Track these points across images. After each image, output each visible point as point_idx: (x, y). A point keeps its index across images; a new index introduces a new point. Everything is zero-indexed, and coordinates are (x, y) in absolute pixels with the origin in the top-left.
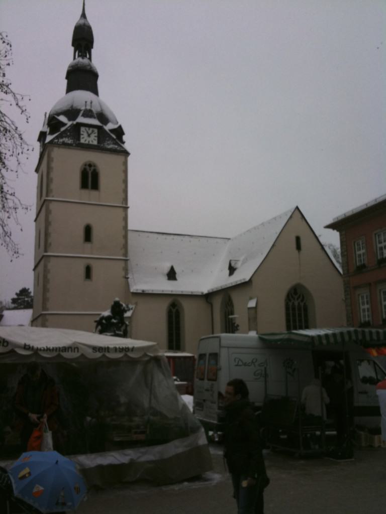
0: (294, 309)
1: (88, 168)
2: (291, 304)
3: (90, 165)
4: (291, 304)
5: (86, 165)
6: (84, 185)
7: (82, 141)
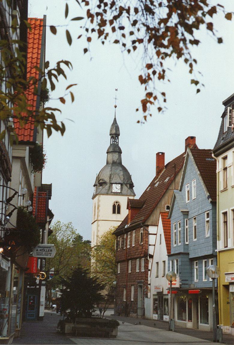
1: (116, 204)
3: (117, 202)
5: (115, 202)
6: (114, 212)
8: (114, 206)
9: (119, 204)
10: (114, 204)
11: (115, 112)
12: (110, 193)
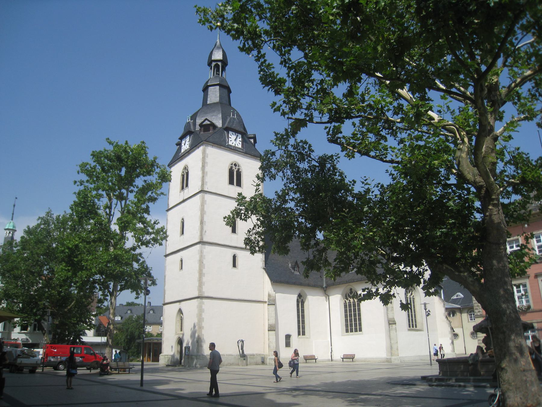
0: (350, 306)
2: (347, 301)
4: (347, 301)
6: (231, 182)
7: (230, 143)
8: (231, 172)
9: (239, 169)
10: (232, 168)
11: (12, 212)
12: (223, 144)
